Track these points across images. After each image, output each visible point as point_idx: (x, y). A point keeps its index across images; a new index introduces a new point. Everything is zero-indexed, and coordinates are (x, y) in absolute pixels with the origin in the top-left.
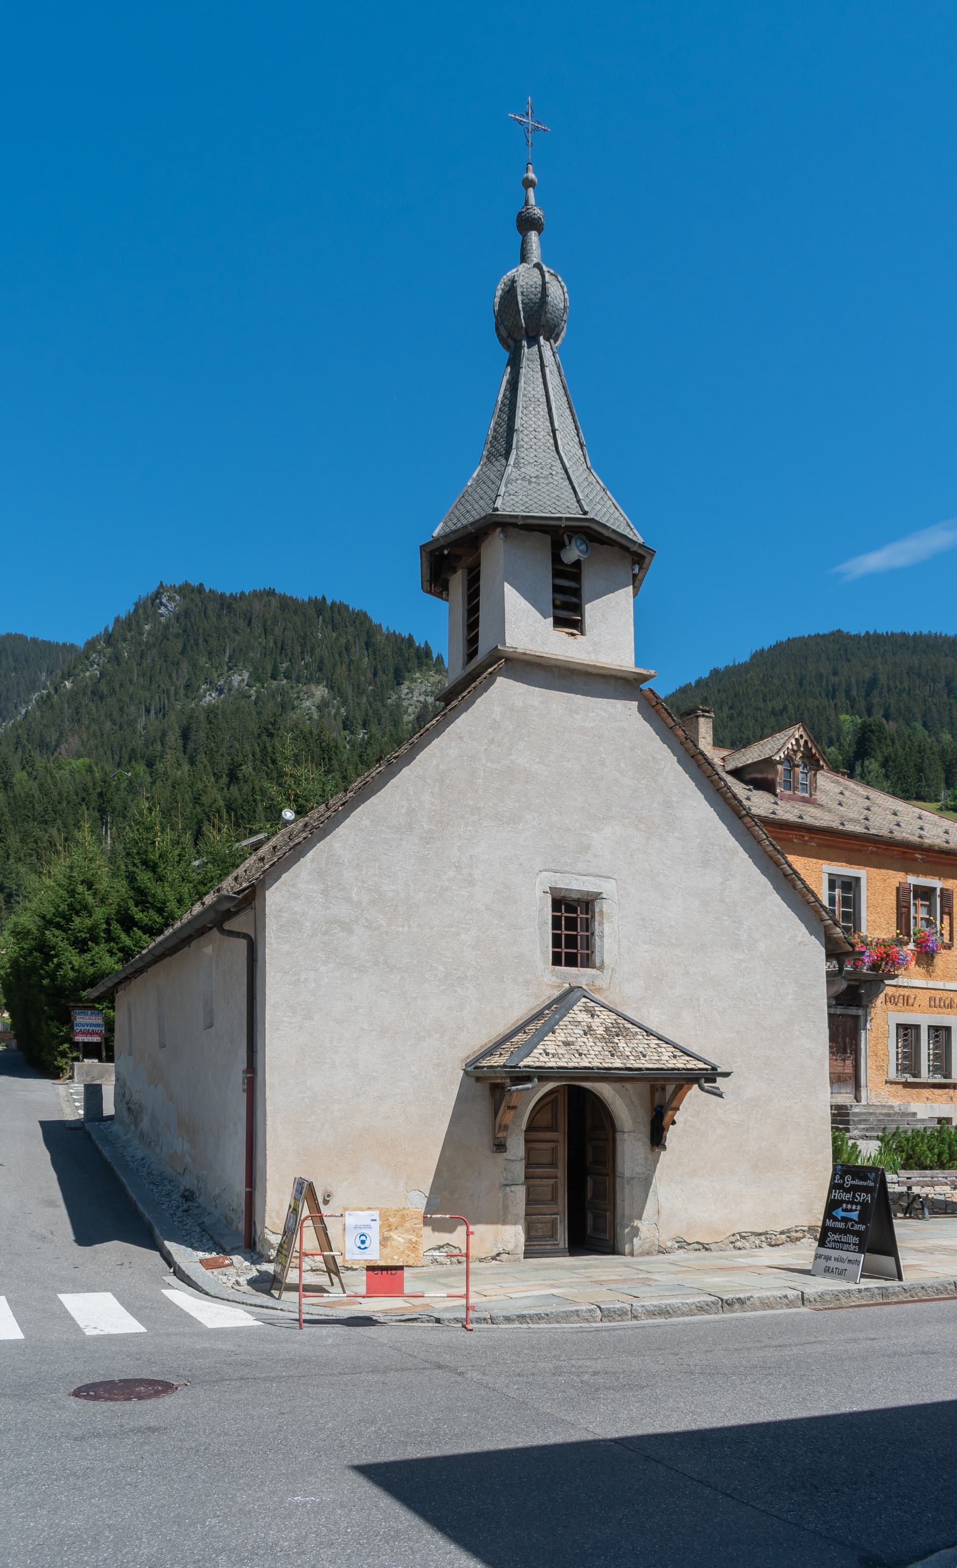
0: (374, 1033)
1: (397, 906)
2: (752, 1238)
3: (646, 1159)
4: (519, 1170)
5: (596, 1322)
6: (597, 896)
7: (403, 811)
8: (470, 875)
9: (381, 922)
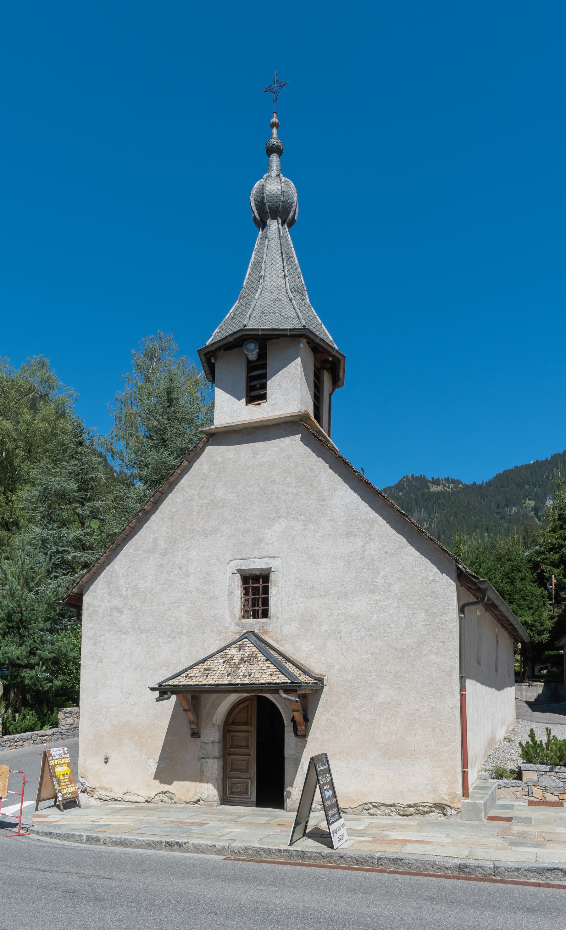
0: (132, 668)
1: (146, 595)
2: (383, 808)
3: (297, 745)
4: (216, 750)
5: (82, 843)
6: (269, 570)
7: (151, 540)
8: (187, 570)
9: (137, 605)
